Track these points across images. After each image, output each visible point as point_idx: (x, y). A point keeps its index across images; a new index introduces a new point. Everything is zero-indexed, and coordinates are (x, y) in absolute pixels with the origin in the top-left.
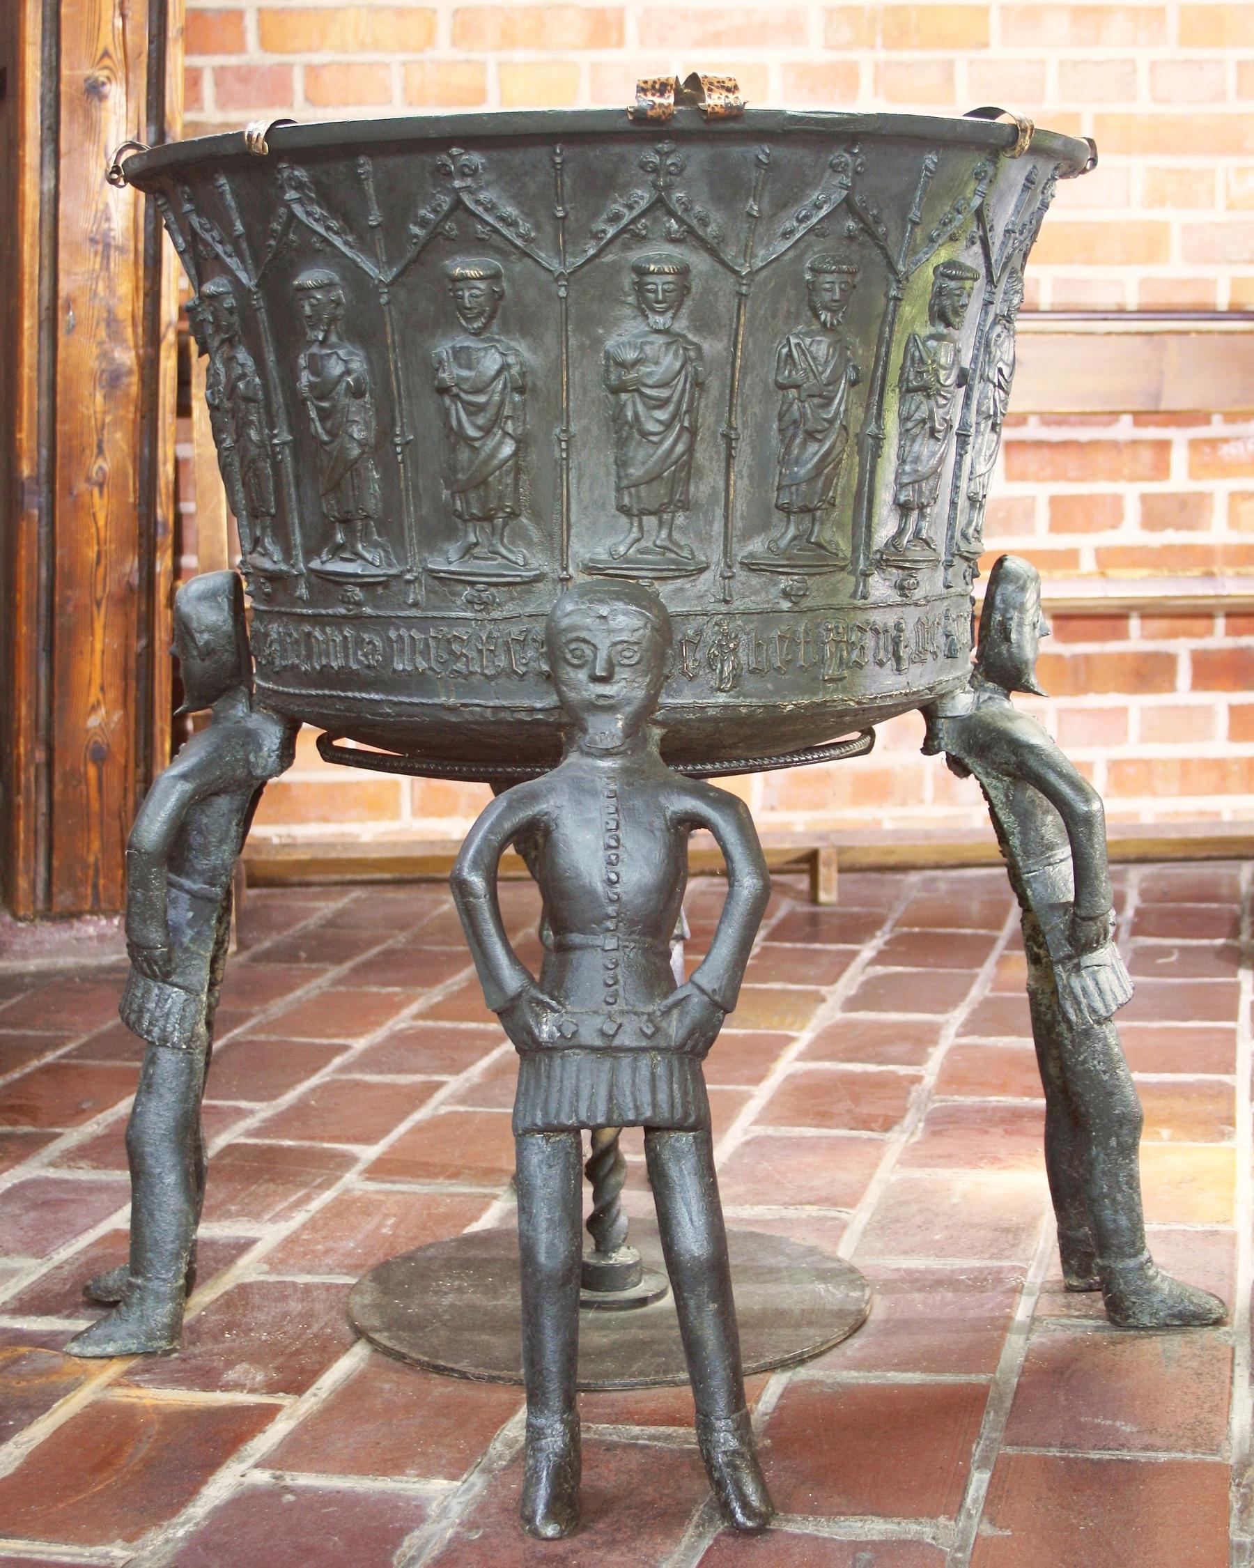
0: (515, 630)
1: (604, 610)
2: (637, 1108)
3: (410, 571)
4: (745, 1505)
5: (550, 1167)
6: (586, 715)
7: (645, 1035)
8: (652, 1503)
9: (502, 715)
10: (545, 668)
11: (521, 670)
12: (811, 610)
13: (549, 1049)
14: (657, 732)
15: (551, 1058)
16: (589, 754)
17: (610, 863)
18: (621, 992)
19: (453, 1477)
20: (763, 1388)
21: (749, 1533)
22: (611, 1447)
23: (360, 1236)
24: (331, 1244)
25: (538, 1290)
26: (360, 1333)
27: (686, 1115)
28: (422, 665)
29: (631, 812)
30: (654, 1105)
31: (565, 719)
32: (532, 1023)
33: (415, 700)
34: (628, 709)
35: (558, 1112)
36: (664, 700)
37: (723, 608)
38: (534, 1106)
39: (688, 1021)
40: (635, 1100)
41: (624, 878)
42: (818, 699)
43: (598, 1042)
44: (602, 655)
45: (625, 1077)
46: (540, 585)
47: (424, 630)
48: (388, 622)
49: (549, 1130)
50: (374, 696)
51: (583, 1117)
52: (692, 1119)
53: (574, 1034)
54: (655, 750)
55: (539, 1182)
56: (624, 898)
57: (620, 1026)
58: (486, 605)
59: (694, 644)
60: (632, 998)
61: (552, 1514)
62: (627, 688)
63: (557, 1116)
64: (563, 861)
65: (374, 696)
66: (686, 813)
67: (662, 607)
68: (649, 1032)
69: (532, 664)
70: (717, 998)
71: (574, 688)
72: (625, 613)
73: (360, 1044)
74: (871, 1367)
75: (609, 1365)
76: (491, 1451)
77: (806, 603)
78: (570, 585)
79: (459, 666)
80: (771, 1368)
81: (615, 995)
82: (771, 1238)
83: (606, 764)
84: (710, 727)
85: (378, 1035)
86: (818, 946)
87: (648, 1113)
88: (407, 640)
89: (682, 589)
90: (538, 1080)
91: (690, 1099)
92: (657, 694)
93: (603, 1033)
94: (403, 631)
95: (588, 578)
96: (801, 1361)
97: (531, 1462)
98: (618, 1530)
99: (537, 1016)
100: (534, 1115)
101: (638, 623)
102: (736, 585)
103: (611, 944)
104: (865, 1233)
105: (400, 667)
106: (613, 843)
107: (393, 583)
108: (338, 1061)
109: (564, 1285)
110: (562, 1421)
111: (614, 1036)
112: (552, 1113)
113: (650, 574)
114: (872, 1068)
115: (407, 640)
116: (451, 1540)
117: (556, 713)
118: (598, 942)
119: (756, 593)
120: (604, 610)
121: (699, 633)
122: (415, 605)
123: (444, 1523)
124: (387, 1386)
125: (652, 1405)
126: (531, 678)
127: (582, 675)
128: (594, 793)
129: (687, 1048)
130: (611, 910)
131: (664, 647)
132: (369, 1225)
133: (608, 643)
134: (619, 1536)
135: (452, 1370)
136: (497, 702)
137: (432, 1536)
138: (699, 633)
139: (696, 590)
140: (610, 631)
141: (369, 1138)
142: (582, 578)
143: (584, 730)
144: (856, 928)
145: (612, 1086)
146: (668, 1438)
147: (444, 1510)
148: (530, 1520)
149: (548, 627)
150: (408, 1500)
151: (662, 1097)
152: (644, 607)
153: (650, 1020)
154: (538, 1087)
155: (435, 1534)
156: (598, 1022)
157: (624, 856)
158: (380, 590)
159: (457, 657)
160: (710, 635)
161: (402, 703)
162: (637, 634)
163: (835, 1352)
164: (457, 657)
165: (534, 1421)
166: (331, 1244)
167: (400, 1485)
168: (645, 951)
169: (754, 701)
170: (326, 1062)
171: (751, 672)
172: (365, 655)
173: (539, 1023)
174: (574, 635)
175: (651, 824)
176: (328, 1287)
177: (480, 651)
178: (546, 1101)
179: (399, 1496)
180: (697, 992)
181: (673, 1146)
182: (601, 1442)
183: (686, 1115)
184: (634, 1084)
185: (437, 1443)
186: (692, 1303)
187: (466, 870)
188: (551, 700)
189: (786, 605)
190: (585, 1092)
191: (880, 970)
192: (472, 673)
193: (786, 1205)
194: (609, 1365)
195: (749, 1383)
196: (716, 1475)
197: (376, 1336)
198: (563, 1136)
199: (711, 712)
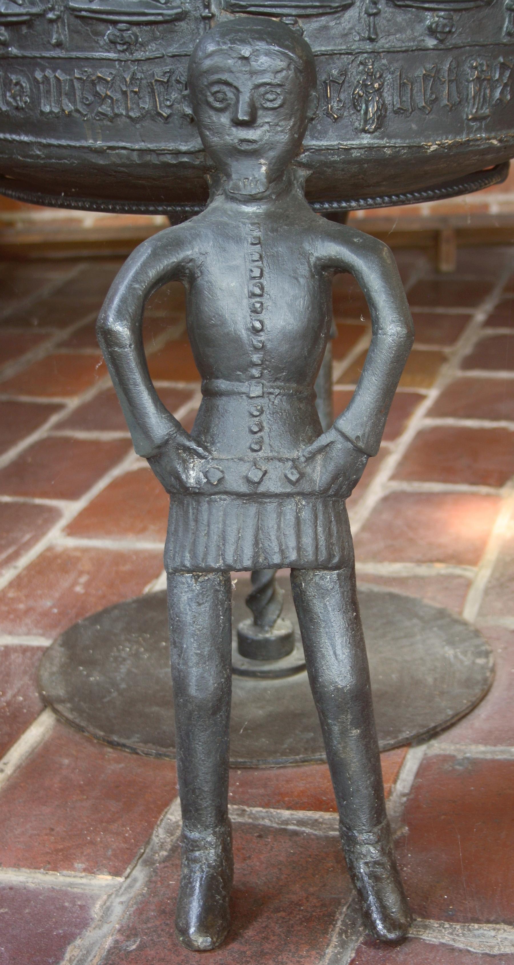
0: (158, 72)
1: (246, 51)
2: (282, 552)
3: (52, 9)
4: (386, 917)
5: (200, 604)
6: (229, 161)
7: (290, 481)
8: (298, 904)
9: (148, 158)
10: (189, 111)
11: (165, 112)
12: (456, 47)
13: (196, 494)
14: (303, 173)
15: (198, 503)
16: (233, 199)
17: (255, 311)
18: (266, 440)
19: (116, 873)
20: (401, 765)
21: (391, 944)
22: (263, 833)
23: (57, 595)
24: (31, 603)
25: (189, 719)
26: (48, 703)
27: (331, 556)
28: (69, 107)
29: (275, 258)
30: (299, 549)
31: (210, 162)
32: (180, 469)
33: (64, 142)
34: (272, 154)
35: (206, 554)
36: (309, 142)
37: (368, 47)
38: (183, 547)
39: (331, 467)
40: (280, 545)
41: (268, 324)
42: (463, 138)
43: (244, 488)
44: (245, 98)
45: (271, 522)
46: (182, 24)
47: (69, 72)
48: (31, 63)
49: (196, 571)
50: (24, 138)
51: (230, 560)
52: (336, 560)
53: (220, 480)
54: (299, 193)
55: (189, 619)
56: (269, 346)
57: (265, 473)
58: (129, 45)
59: (338, 84)
60: (276, 444)
61: (204, 926)
62: (270, 132)
63: (205, 559)
64: (207, 309)
65: (24, 138)
66: (330, 259)
67: (306, 47)
68: (294, 478)
69: (176, 106)
70: (360, 444)
71: (218, 131)
72: (268, 54)
73: (73, 403)
74: (498, 741)
75: (264, 741)
76: (155, 840)
77: (454, 40)
78: (213, 24)
79: (105, 108)
80: (408, 744)
81: (260, 442)
82: (406, 600)
83: (250, 209)
84: (354, 168)
85: (89, 395)
86: (440, 310)
87: (293, 556)
88: (52, 81)
89: (325, 28)
90: (186, 524)
91: (334, 540)
92: (302, 136)
93: (248, 480)
94: (48, 73)
95: (231, 17)
96: (433, 734)
97: (186, 871)
98: (266, 938)
99: (184, 461)
100: (183, 557)
101: (281, 64)
102: (381, 22)
103: (256, 391)
104: (487, 592)
105: (47, 109)
106: (257, 291)
107: (37, 22)
108: (54, 419)
109: (214, 713)
110: (214, 833)
111: (259, 483)
112: (201, 555)
113: (294, 12)
114: (488, 424)
115: (52, 81)
116: (110, 952)
117: (201, 157)
118: (243, 390)
119: (401, 30)
120: (246, 51)
121: (344, 73)
122: (59, 45)
123: (106, 928)
124: (66, 761)
125: (301, 785)
126: (176, 120)
127: (225, 119)
128: (238, 240)
129: (331, 492)
130: (256, 358)
131: (308, 82)
132: (65, 583)
133: (250, 85)
134: (267, 946)
135: (124, 746)
136: (142, 145)
137: (93, 944)
138: (344, 73)
139: (340, 28)
140: (253, 73)
141: (73, 494)
142: (225, 17)
143: (229, 176)
144: (472, 295)
145: (258, 529)
146: (315, 823)
147: (107, 910)
148: (184, 932)
149: (190, 69)
150: (74, 898)
151: (307, 541)
152: (287, 47)
153: (295, 467)
154: (186, 530)
155: (100, 937)
156: (244, 469)
157: (268, 303)
158: (24, 30)
159: (103, 99)
160: (356, 75)
161: (50, 145)
162: (280, 76)
163: (464, 724)
164: (103, 99)
165: (188, 834)
166: (31, 603)
167: (68, 880)
168: (290, 396)
169: (398, 142)
170: (45, 420)
171: (396, 112)
172: (14, 97)
173: (186, 469)
174: (216, 77)
175: (295, 271)
176: (25, 650)
177: (124, 93)
178: (194, 544)
179: (66, 893)
180: (340, 438)
181: (317, 584)
182: (253, 827)
183: (331, 556)
184: (279, 528)
185: (105, 830)
186: (336, 729)
187: (111, 319)
188: (195, 144)
189: (431, 43)
190: (231, 538)
191: (490, 332)
192: (117, 115)
193: (419, 562)
194: (264, 741)
195: (387, 761)
196: (359, 884)
197: (60, 707)
198: (211, 576)
199: (355, 154)
